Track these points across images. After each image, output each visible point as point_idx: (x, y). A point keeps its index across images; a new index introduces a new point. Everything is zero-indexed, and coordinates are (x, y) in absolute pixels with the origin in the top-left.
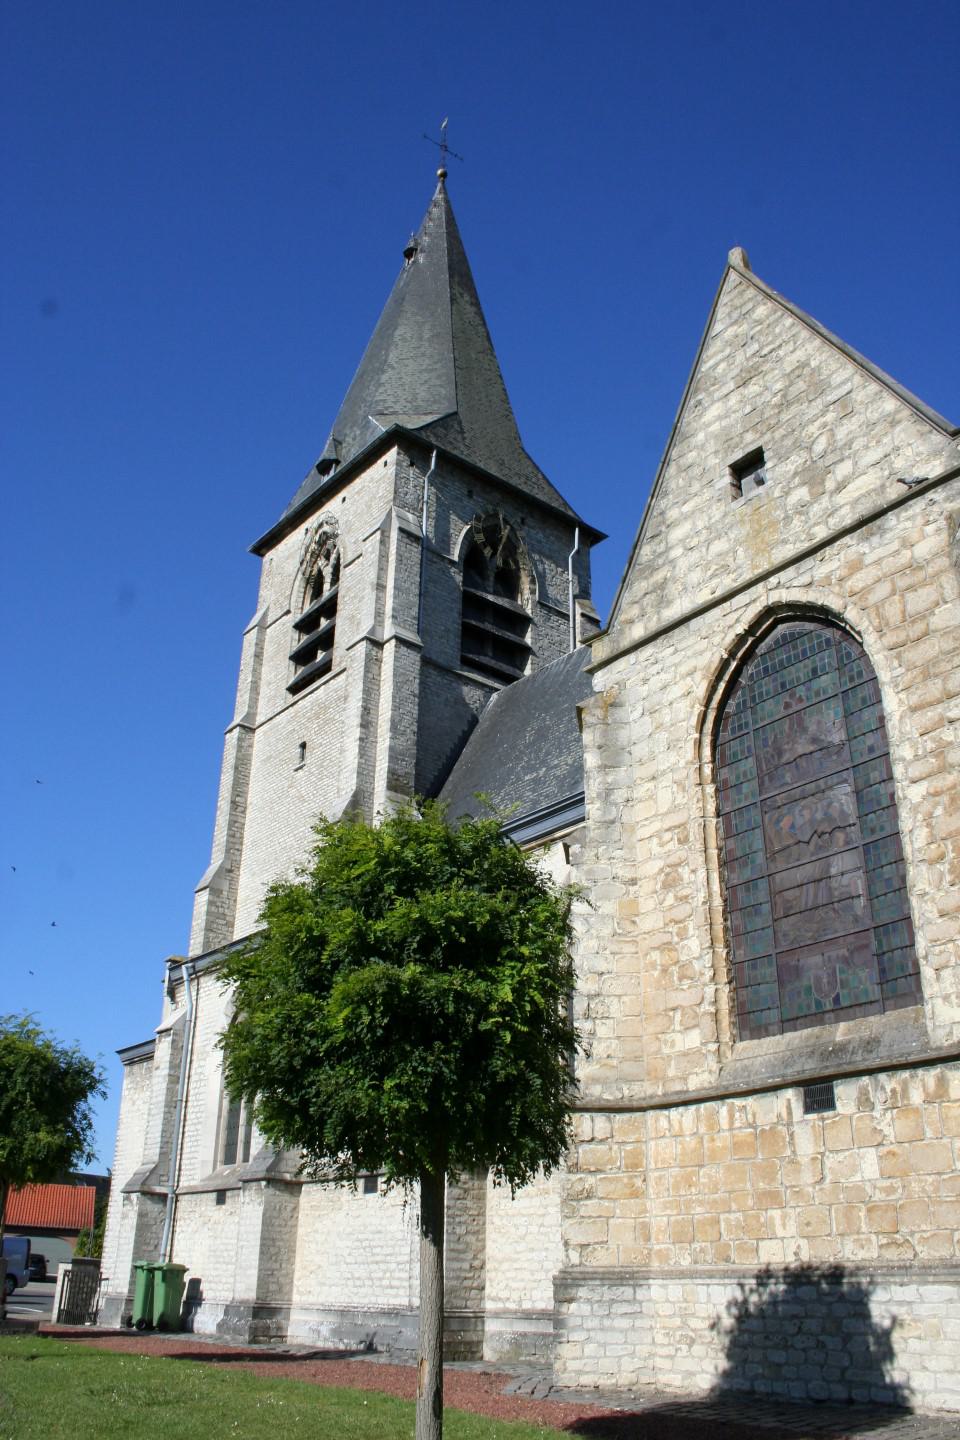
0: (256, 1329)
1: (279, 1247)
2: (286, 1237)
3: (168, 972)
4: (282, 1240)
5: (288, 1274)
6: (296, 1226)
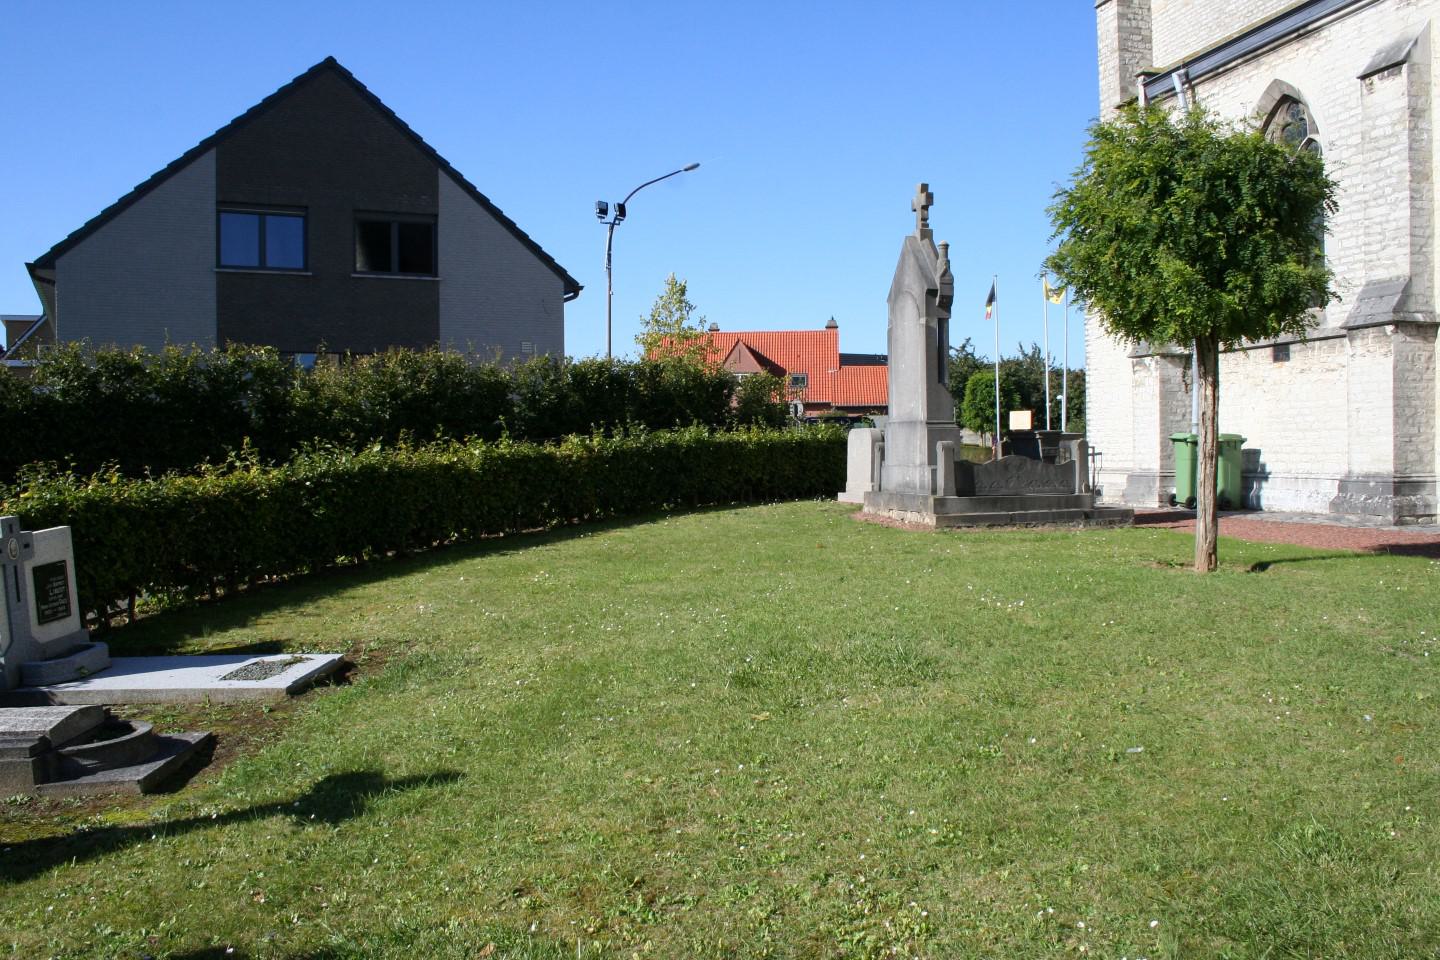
0: (1401, 507)
1: (1416, 407)
2: (1422, 394)
3: (1142, 87)
4: (1419, 398)
5: (1428, 441)
6: (1433, 380)
